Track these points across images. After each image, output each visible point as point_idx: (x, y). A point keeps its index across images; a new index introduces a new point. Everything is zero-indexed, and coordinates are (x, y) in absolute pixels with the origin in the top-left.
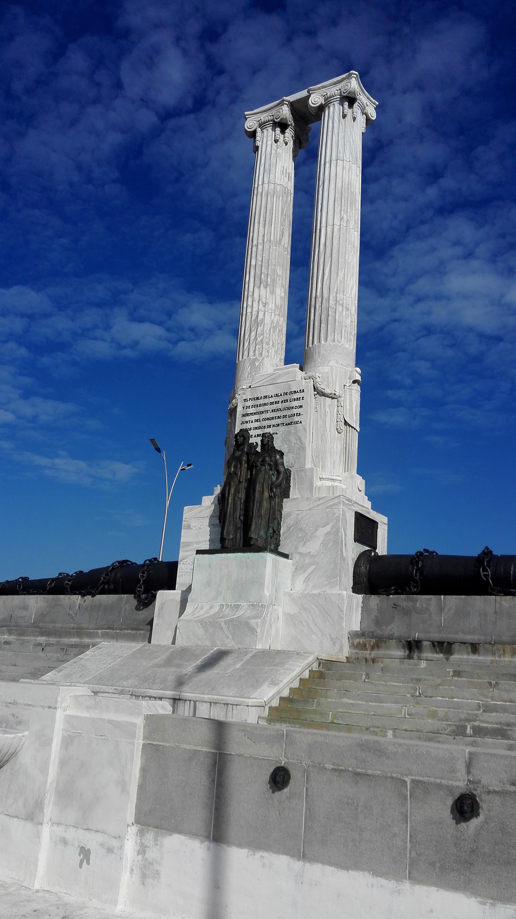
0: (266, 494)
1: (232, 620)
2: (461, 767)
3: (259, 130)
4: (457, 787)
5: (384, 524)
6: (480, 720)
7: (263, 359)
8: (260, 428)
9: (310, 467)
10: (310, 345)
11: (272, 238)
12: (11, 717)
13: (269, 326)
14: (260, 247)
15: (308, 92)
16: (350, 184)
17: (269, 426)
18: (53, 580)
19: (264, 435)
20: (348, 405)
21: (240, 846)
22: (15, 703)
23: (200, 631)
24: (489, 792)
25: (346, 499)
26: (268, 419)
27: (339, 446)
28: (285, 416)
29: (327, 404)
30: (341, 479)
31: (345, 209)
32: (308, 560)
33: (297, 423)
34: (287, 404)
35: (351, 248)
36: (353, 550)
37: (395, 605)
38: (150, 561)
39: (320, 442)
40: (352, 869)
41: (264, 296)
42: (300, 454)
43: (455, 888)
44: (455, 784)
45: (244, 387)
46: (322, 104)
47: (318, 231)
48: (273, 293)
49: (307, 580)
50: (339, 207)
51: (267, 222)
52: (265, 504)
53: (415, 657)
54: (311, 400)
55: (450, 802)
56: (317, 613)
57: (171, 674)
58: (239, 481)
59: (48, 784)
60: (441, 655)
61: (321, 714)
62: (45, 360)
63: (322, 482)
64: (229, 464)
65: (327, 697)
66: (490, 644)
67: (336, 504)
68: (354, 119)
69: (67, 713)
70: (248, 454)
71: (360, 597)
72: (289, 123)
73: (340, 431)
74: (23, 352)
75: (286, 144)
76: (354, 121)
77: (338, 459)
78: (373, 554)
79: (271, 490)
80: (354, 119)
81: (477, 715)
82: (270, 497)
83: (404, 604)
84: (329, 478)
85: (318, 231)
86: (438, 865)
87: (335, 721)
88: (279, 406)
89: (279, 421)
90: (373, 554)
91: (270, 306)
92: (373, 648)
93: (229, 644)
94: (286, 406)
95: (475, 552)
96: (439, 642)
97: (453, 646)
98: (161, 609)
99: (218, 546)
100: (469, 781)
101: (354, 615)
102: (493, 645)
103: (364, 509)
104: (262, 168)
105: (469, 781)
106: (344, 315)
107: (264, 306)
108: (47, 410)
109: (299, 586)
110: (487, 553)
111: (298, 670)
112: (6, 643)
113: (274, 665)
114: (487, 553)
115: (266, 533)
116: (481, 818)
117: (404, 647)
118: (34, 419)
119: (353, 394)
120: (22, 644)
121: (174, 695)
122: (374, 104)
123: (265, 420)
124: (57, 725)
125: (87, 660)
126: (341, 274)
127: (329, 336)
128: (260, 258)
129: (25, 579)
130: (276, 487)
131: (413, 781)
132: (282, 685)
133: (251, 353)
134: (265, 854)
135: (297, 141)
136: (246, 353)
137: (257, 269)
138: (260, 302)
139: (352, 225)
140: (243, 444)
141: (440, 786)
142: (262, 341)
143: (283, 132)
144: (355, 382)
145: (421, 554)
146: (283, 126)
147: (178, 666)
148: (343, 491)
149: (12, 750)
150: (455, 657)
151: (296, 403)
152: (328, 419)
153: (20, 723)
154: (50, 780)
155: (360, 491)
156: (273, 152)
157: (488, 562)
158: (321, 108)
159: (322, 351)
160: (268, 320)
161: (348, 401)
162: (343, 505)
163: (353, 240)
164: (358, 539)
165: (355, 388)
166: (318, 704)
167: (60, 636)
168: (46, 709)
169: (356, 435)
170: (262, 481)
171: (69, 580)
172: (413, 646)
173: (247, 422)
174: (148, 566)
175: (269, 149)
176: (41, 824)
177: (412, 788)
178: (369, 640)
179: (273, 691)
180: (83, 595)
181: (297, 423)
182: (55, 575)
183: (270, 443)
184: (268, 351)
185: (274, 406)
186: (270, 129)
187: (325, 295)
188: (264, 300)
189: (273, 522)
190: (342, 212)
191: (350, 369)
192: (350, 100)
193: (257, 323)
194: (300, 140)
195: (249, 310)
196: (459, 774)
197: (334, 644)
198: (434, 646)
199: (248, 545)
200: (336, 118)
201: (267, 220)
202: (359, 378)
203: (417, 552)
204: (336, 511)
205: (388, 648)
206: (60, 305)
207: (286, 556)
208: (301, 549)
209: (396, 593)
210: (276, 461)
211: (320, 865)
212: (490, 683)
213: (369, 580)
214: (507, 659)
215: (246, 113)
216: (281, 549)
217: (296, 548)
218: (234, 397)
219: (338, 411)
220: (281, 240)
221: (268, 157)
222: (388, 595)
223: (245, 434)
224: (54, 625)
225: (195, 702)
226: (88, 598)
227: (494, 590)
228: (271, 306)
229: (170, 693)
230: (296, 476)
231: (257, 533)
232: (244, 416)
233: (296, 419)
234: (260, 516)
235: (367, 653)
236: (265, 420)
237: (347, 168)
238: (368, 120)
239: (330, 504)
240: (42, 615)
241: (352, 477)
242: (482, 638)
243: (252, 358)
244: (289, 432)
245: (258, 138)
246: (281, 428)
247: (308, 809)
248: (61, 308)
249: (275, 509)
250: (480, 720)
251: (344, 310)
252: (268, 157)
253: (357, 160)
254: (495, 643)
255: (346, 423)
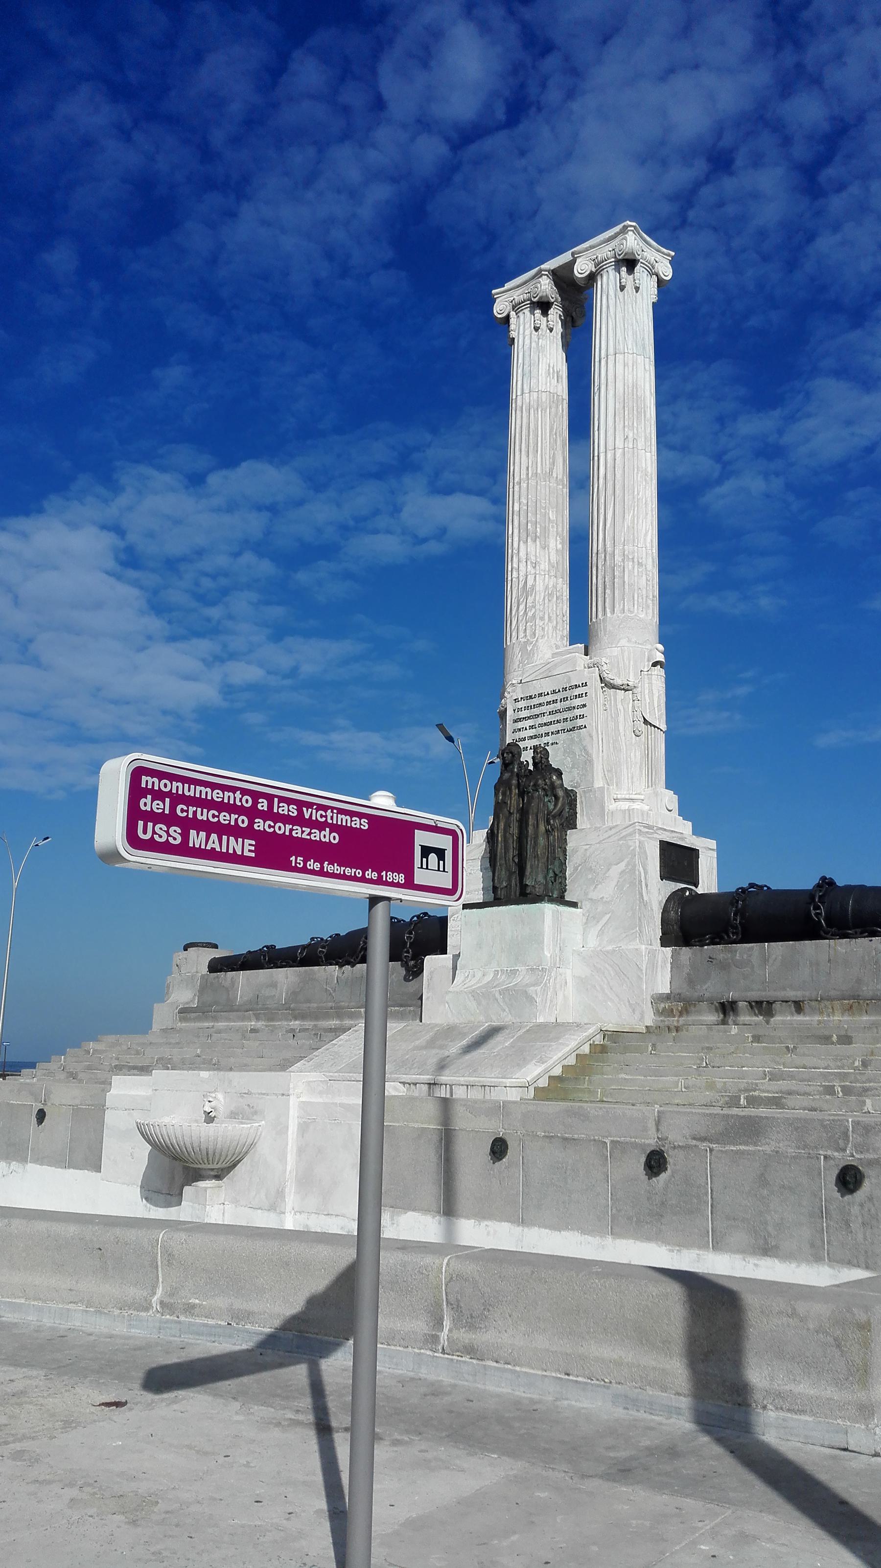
0: (542, 828)
1: (507, 989)
2: (651, 1125)
3: (513, 314)
4: (649, 1145)
5: (713, 850)
6: (759, 1090)
7: (537, 641)
8: (535, 737)
9: (601, 785)
10: (594, 620)
11: (539, 471)
12: (246, 1107)
13: (543, 594)
14: (524, 485)
15: (573, 254)
16: (635, 386)
17: (547, 734)
18: (304, 947)
19: (535, 748)
20: (647, 696)
21: (468, 1217)
22: (249, 1093)
23: (472, 1005)
24: (674, 1148)
25: (645, 827)
26: (545, 724)
27: (638, 754)
28: (565, 720)
29: (619, 700)
30: (642, 797)
31: (630, 424)
32: (600, 908)
33: (580, 728)
34: (567, 704)
35: (641, 477)
36: (658, 891)
37: (710, 958)
38: (418, 916)
39: (612, 750)
40: (564, 1230)
41: (534, 553)
42: (586, 771)
43: (649, 1239)
44: (647, 1142)
45: (514, 682)
46: (591, 271)
47: (596, 458)
48: (545, 547)
49: (601, 933)
50: (622, 422)
51: (531, 448)
52: (542, 841)
53: (730, 1022)
54: (596, 695)
55: (643, 1159)
56: (613, 974)
57: (433, 1057)
58: (510, 812)
59: (288, 1173)
60: (761, 1018)
61: (590, 1091)
62: (302, 577)
63: (617, 803)
64: (497, 788)
65: (603, 1074)
66: (817, 1000)
67: (630, 834)
68: (637, 289)
69: (301, 1099)
70: (518, 775)
71: (669, 950)
72: (552, 300)
73: (638, 734)
74: (266, 567)
75: (551, 330)
76: (637, 292)
77: (638, 772)
78: (687, 894)
79: (548, 823)
80: (637, 289)
81: (756, 1084)
82: (547, 831)
83: (721, 956)
84: (628, 799)
85: (596, 458)
86: (635, 1219)
87: (605, 1099)
88: (558, 706)
89: (559, 727)
90: (687, 894)
91: (542, 567)
92: (681, 1014)
93: (506, 1018)
94: (565, 707)
95: (807, 882)
96: (757, 1002)
97: (774, 1005)
98: (431, 979)
99: (491, 897)
100: (658, 1138)
101: (659, 974)
102: (819, 1001)
103: (674, 835)
104: (520, 371)
105: (658, 1138)
106: (636, 574)
107: (534, 568)
108: (313, 656)
109: (593, 942)
110: (827, 884)
111: (573, 1044)
112: (253, 1031)
113: (548, 1041)
114: (827, 884)
115: (545, 878)
116: (669, 1171)
117: (717, 1010)
118: (293, 672)
119: (654, 682)
120: (272, 1031)
121: (429, 1079)
122: (669, 255)
123: (541, 725)
124: (291, 1113)
125: (340, 1046)
126: (629, 517)
127: (617, 605)
128: (524, 501)
129: (271, 948)
130: (554, 817)
131: (612, 1142)
132: (551, 1062)
133: (521, 634)
134: (489, 1223)
135: (569, 319)
136: (514, 634)
137: (521, 516)
138: (529, 563)
139: (641, 444)
140: (512, 763)
141: (635, 1145)
142: (534, 616)
143: (545, 313)
144: (655, 664)
145: (744, 890)
146: (544, 306)
147: (441, 1047)
148: (642, 815)
149: (249, 1141)
150: (777, 1019)
151: (578, 702)
152: (621, 718)
153: (256, 1113)
154: (289, 1168)
155: (670, 811)
156: (534, 345)
157: (820, 897)
158: (592, 278)
159: (609, 627)
160: (540, 587)
161: (647, 692)
162: (640, 835)
163: (644, 465)
164: (667, 873)
165: (656, 673)
166: (590, 1081)
167: (317, 1018)
168: (280, 1097)
169: (662, 737)
170: (535, 811)
171: (323, 947)
172: (727, 1008)
173: (520, 730)
174: (416, 924)
175: (527, 342)
176: (284, 1213)
177: (611, 1149)
178: (676, 1005)
179: (539, 1069)
180: (341, 966)
181: (580, 728)
182: (306, 941)
183: (544, 760)
184: (543, 629)
185: (552, 707)
186: (527, 311)
187: (609, 549)
188: (533, 558)
189: (552, 863)
190: (626, 429)
191: (649, 647)
192: (630, 263)
193: (527, 592)
194: (572, 318)
195: (515, 574)
196: (650, 1133)
197: (634, 1011)
198: (752, 1007)
199: (524, 895)
200: (612, 293)
201: (531, 445)
202: (661, 657)
203: (738, 889)
204: (630, 843)
205: (699, 1012)
206: (317, 483)
207: (574, 905)
208: (593, 895)
209: (713, 943)
210: (552, 784)
211: (536, 1228)
212: (787, 1048)
213: (682, 928)
214: (836, 1018)
215: (494, 292)
216: (568, 898)
217: (586, 894)
218: (502, 697)
219: (633, 706)
220: (551, 470)
221: (527, 354)
222: (702, 946)
223: (514, 749)
224: (308, 1005)
225: (451, 1086)
226: (347, 968)
227: (827, 933)
228: (544, 566)
229: (426, 1078)
230: (583, 799)
231: (535, 879)
232: (515, 721)
233: (580, 722)
234: (536, 856)
235: (674, 1021)
236: (541, 725)
237: (630, 364)
238: (660, 282)
239: (624, 834)
240: (294, 993)
241: (656, 794)
242: (807, 994)
243: (523, 640)
244: (572, 740)
245: (512, 327)
246: (562, 736)
247: (525, 1176)
248: (319, 488)
249: (554, 846)
250: (759, 1090)
251: (636, 566)
252: (527, 354)
253: (644, 348)
254: (822, 999)
255: (646, 722)
